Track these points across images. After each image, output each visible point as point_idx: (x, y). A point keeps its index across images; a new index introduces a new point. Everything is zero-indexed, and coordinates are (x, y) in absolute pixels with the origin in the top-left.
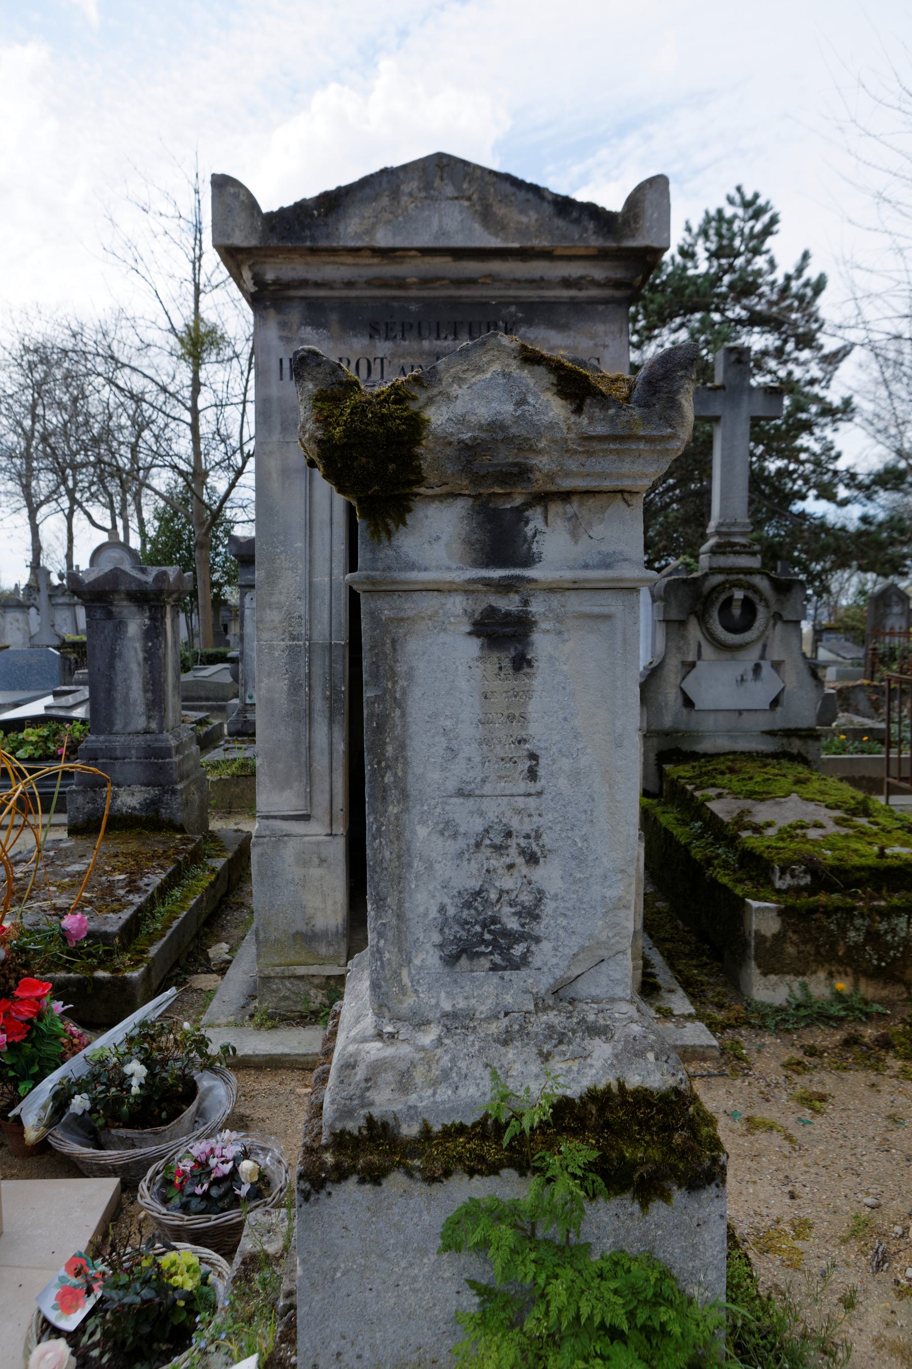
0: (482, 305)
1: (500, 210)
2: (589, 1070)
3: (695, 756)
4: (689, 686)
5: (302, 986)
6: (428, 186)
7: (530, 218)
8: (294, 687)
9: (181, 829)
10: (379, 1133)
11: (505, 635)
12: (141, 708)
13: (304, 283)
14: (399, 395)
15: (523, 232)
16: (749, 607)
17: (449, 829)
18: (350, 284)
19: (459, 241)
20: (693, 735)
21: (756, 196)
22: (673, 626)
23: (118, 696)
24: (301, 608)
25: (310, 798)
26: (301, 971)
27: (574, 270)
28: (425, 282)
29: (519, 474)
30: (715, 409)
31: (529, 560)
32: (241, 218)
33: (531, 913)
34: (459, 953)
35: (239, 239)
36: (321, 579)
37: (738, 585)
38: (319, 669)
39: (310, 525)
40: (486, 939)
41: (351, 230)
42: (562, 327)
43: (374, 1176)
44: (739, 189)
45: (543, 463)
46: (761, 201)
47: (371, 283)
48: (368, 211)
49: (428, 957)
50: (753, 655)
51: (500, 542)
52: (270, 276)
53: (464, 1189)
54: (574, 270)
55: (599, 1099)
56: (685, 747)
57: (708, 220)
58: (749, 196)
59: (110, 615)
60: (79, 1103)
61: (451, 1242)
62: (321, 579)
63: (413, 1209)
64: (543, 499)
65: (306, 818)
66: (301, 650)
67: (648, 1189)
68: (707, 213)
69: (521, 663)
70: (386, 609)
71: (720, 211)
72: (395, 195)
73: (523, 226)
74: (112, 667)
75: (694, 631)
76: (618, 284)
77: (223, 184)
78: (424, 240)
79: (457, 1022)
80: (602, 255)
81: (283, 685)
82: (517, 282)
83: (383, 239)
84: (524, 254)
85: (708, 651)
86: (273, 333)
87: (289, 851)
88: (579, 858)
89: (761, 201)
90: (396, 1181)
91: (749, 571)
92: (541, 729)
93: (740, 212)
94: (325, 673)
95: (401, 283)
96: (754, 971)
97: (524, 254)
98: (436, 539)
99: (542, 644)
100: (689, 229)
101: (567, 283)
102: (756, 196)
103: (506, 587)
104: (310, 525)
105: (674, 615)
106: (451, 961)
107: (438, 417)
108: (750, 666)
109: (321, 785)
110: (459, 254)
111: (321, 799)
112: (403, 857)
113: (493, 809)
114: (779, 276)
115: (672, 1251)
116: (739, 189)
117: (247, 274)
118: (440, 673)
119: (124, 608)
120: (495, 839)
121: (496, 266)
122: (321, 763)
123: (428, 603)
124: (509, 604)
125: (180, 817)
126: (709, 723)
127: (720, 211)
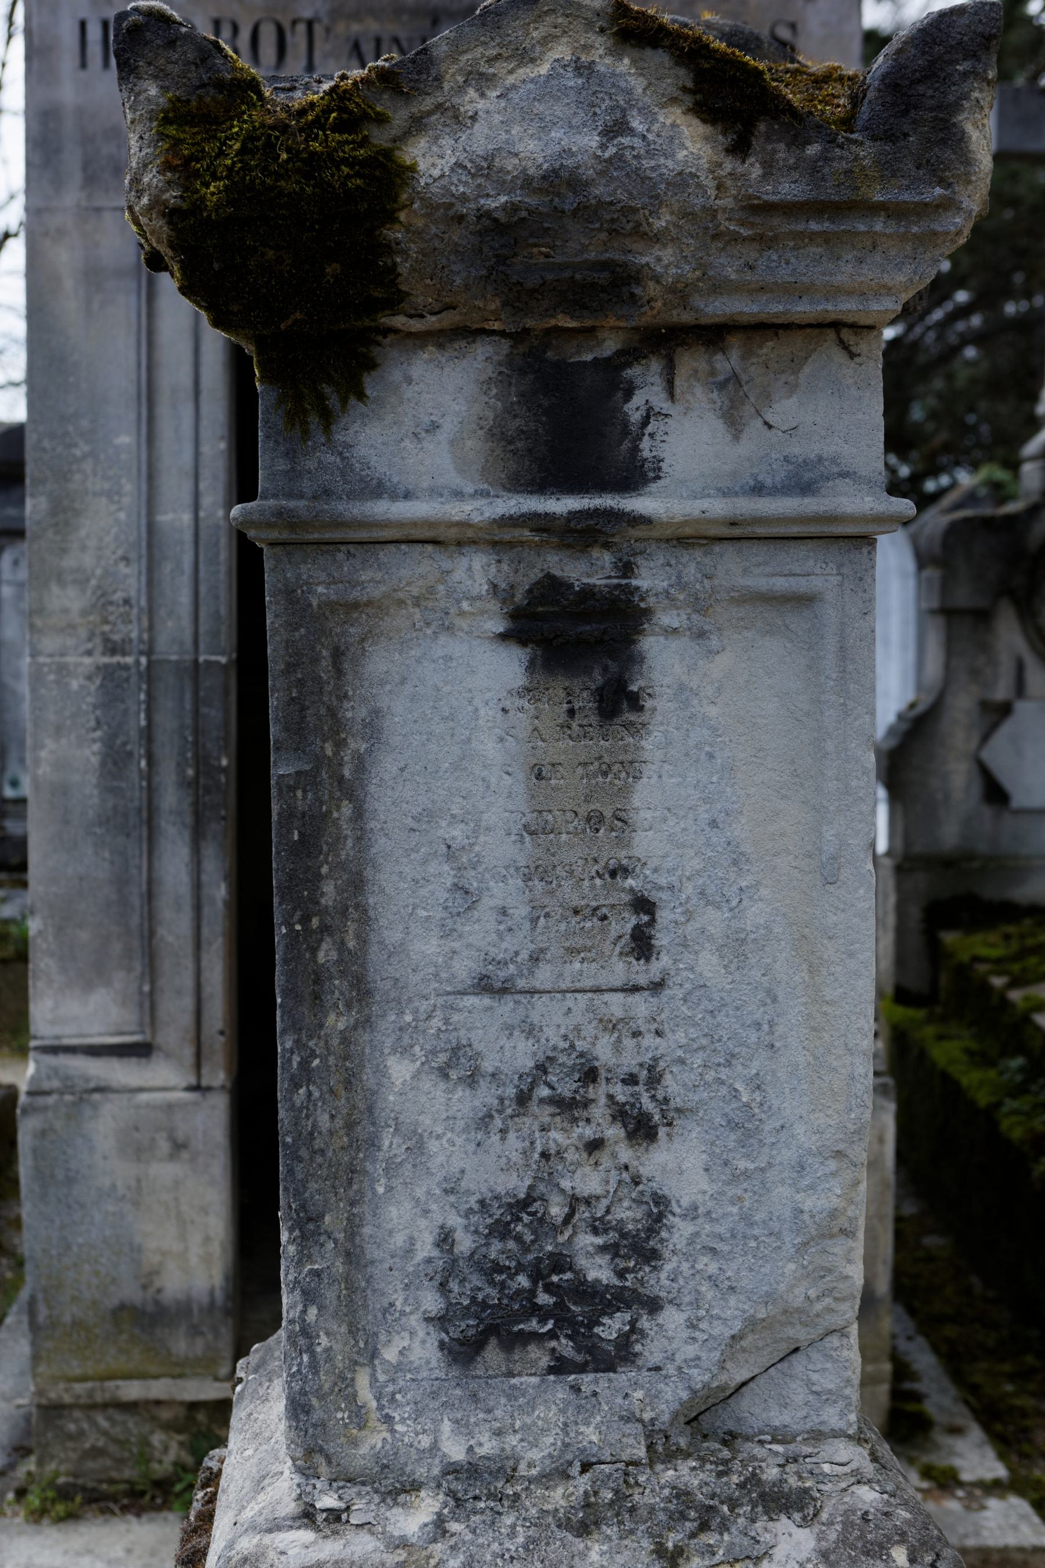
4: (999, 755)
5: (132, 1423)
8: (114, 759)
11: (581, 644)
14: (347, 111)
17: (458, 1064)
20: (1006, 866)
24: (130, 580)
25: (149, 1007)
26: (132, 1391)
29: (613, 285)
31: (636, 475)
33: (639, 1247)
36: (175, 517)
39: (149, 395)
51: (569, 438)
56: (990, 892)
62: (175, 517)
64: (666, 341)
65: (141, 1051)
69: (618, 702)
87: (105, 1125)
88: (745, 1126)
98: (429, 432)
99: (664, 660)
103: (582, 534)
104: (149, 395)
105: (964, 597)
106: (463, 1352)
107: (433, 160)
111: (176, 1009)
112: (360, 1126)
113: (556, 1020)
118: (445, 716)
120: (562, 1087)
122: (175, 927)
123: (414, 570)
124: (590, 571)
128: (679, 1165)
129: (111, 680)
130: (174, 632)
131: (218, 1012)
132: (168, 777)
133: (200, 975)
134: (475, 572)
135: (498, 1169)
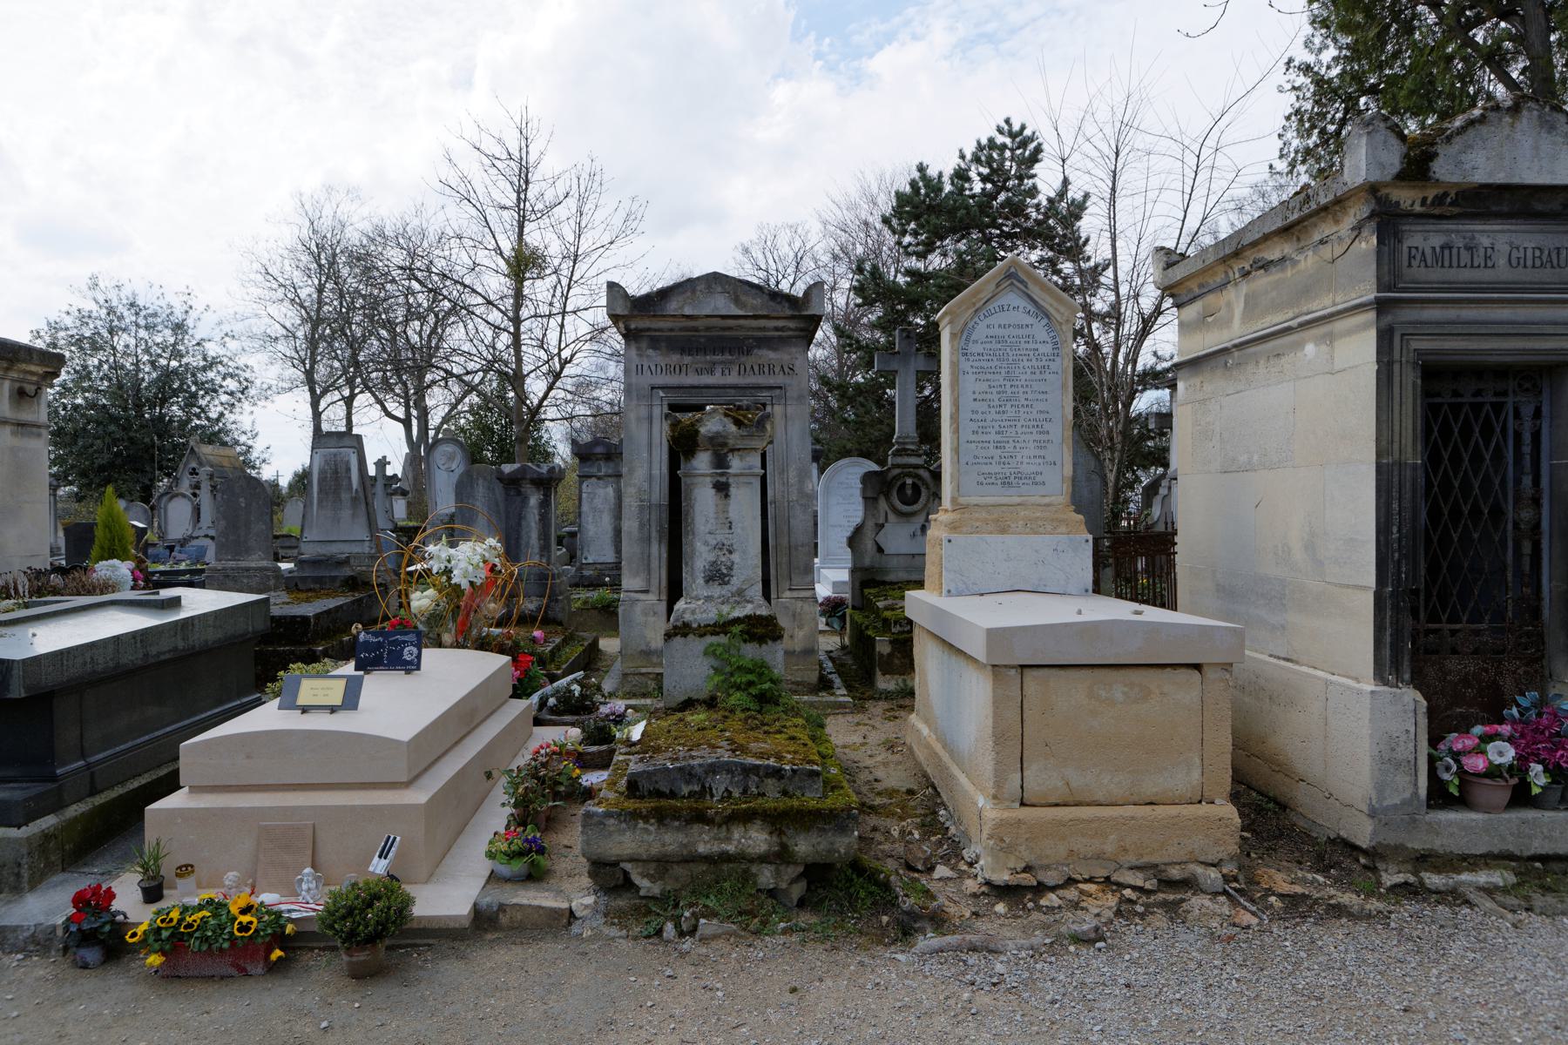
0: (736, 339)
1: (743, 298)
2: (748, 610)
3: (884, 583)
4: (881, 539)
5: (643, 679)
6: (709, 287)
7: (757, 302)
8: (642, 526)
9: (560, 624)
10: (686, 625)
11: (722, 488)
12: (536, 550)
13: (649, 329)
14: (692, 425)
15: (754, 308)
16: (916, 490)
17: (706, 543)
18: (671, 330)
19: (724, 312)
20: (884, 571)
21: (1023, 127)
22: (869, 501)
23: (523, 542)
24: (646, 485)
25: (649, 581)
26: (644, 670)
27: (780, 323)
28: (708, 329)
29: (725, 444)
30: (894, 366)
31: (728, 467)
32: (621, 302)
33: (730, 568)
34: (709, 579)
35: (619, 311)
36: (656, 472)
37: (909, 475)
38: (654, 517)
39: (650, 445)
40: (717, 575)
41: (673, 306)
42: (775, 350)
43: (685, 635)
44: (1007, 121)
45: (731, 442)
46: (1027, 132)
47: (681, 329)
48: (680, 299)
49: (700, 581)
50: (920, 519)
51: (720, 462)
52: (633, 326)
53: (710, 639)
54: (780, 323)
55: (748, 617)
56: (878, 578)
57: (980, 147)
58: (1016, 128)
59: (519, 493)
60: (552, 701)
61: (705, 654)
62: (656, 472)
63: (697, 645)
64: (732, 450)
65: (646, 592)
66: (645, 507)
67: (761, 640)
68: (979, 143)
69: (727, 496)
70: (688, 481)
71: (991, 140)
72: (694, 291)
73: (755, 303)
74: (519, 524)
75: (883, 504)
76: (801, 330)
77: (612, 286)
78: (707, 311)
79: (708, 599)
80: (792, 317)
81: (636, 524)
82: (753, 329)
83: (688, 311)
84: (755, 317)
85: (891, 517)
86: (633, 352)
87: (638, 608)
88: (744, 552)
89: (1027, 132)
90: (691, 636)
91: (917, 467)
92: (733, 515)
93: (1008, 141)
94: (659, 518)
95: (696, 329)
96: (879, 673)
97: (755, 317)
98: (702, 462)
99: (733, 491)
100: (963, 157)
101: (777, 329)
102: (1023, 127)
103: (722, 474)
104: (650, 445)
105: (869, 494)
106: (707, 582)
107: (702, 430)
108: (919, 526)
109: (655, 575)
110: (723, 317)
111: (655, 582)
112: (693, 551)
113: (719, 538)
114: (1042, 199)
115: (768, 659)
116: (1007, 121)
117: (621, 325)
118: (703, 500)
119: (528, 489)
120: (720, 547)
121: (742, 322)
122: (655, 564)
123: (700, 479)
124: (723, 479)
125: (560, 616)
126: (894, 562)
127: (991, 140)
128: (735, 557)
129: (641, 508)
130: (655, 498)
131: (664, 583)
132: (653, 529)
133: (660, 574)
134: (708, 479)
135: (711, 557)
